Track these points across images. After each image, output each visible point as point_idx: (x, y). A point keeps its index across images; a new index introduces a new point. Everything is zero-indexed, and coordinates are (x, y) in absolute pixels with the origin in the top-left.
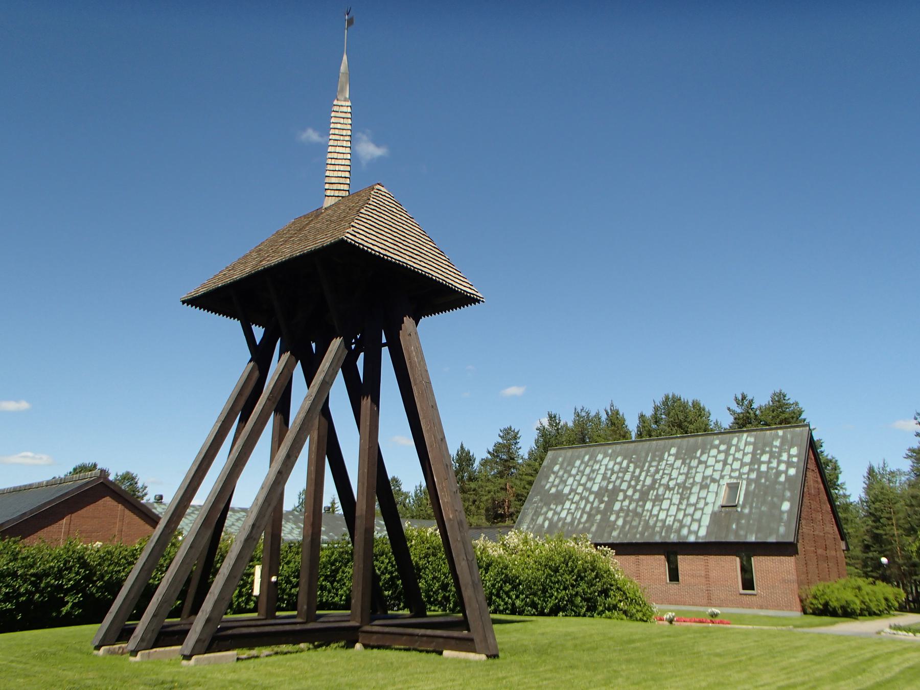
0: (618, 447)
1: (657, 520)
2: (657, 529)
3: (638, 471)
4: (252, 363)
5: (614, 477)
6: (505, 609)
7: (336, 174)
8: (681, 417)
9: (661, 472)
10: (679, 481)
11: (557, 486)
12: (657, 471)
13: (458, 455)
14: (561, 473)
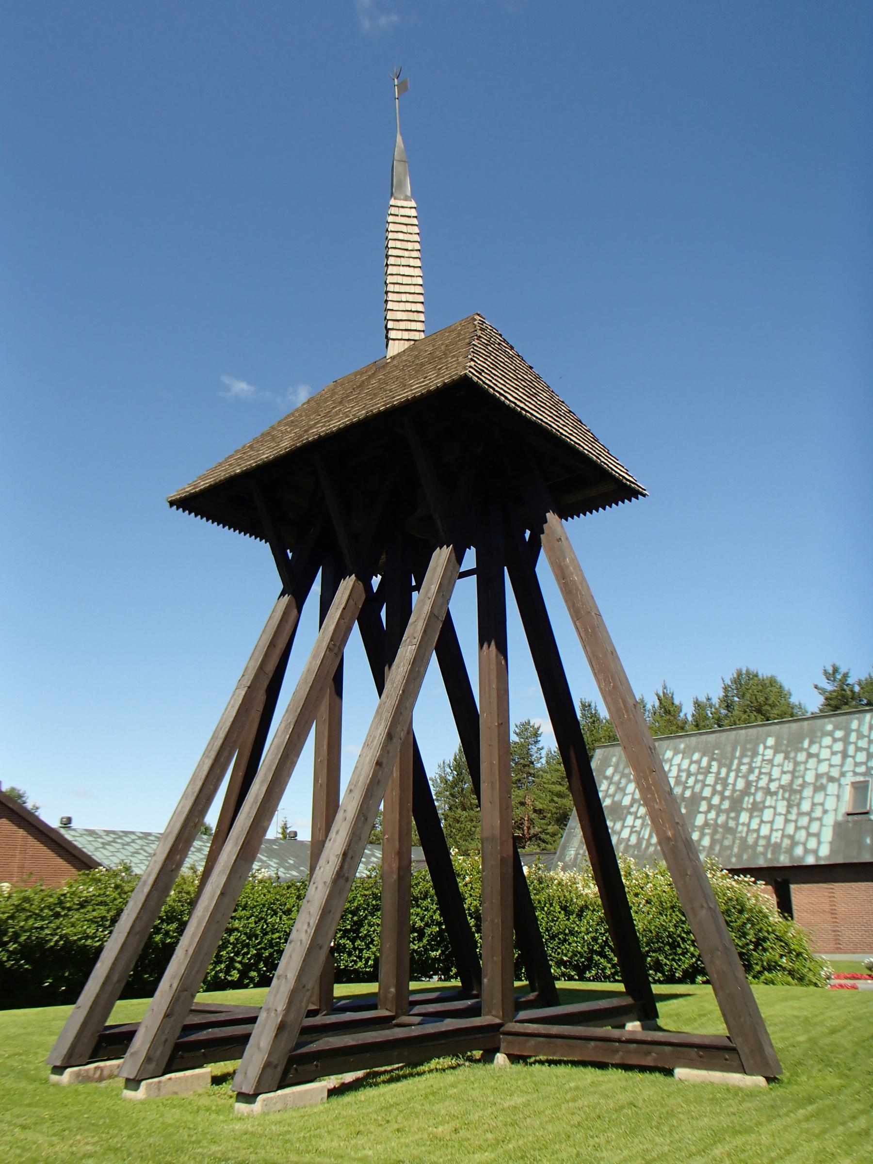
0: (693, 740)
1: (758, 837)
2: (760, 849)
3: (724, 771)
4: (286, 598)
5: (691, 781)
6: (613, 974)
7: (402, 306)
8: (761, 700)
9: (757, 771)
10: (783, 782)
11: (613, 796)
12: (751, 770)
13: (455, 760)
14: (616, 778)
